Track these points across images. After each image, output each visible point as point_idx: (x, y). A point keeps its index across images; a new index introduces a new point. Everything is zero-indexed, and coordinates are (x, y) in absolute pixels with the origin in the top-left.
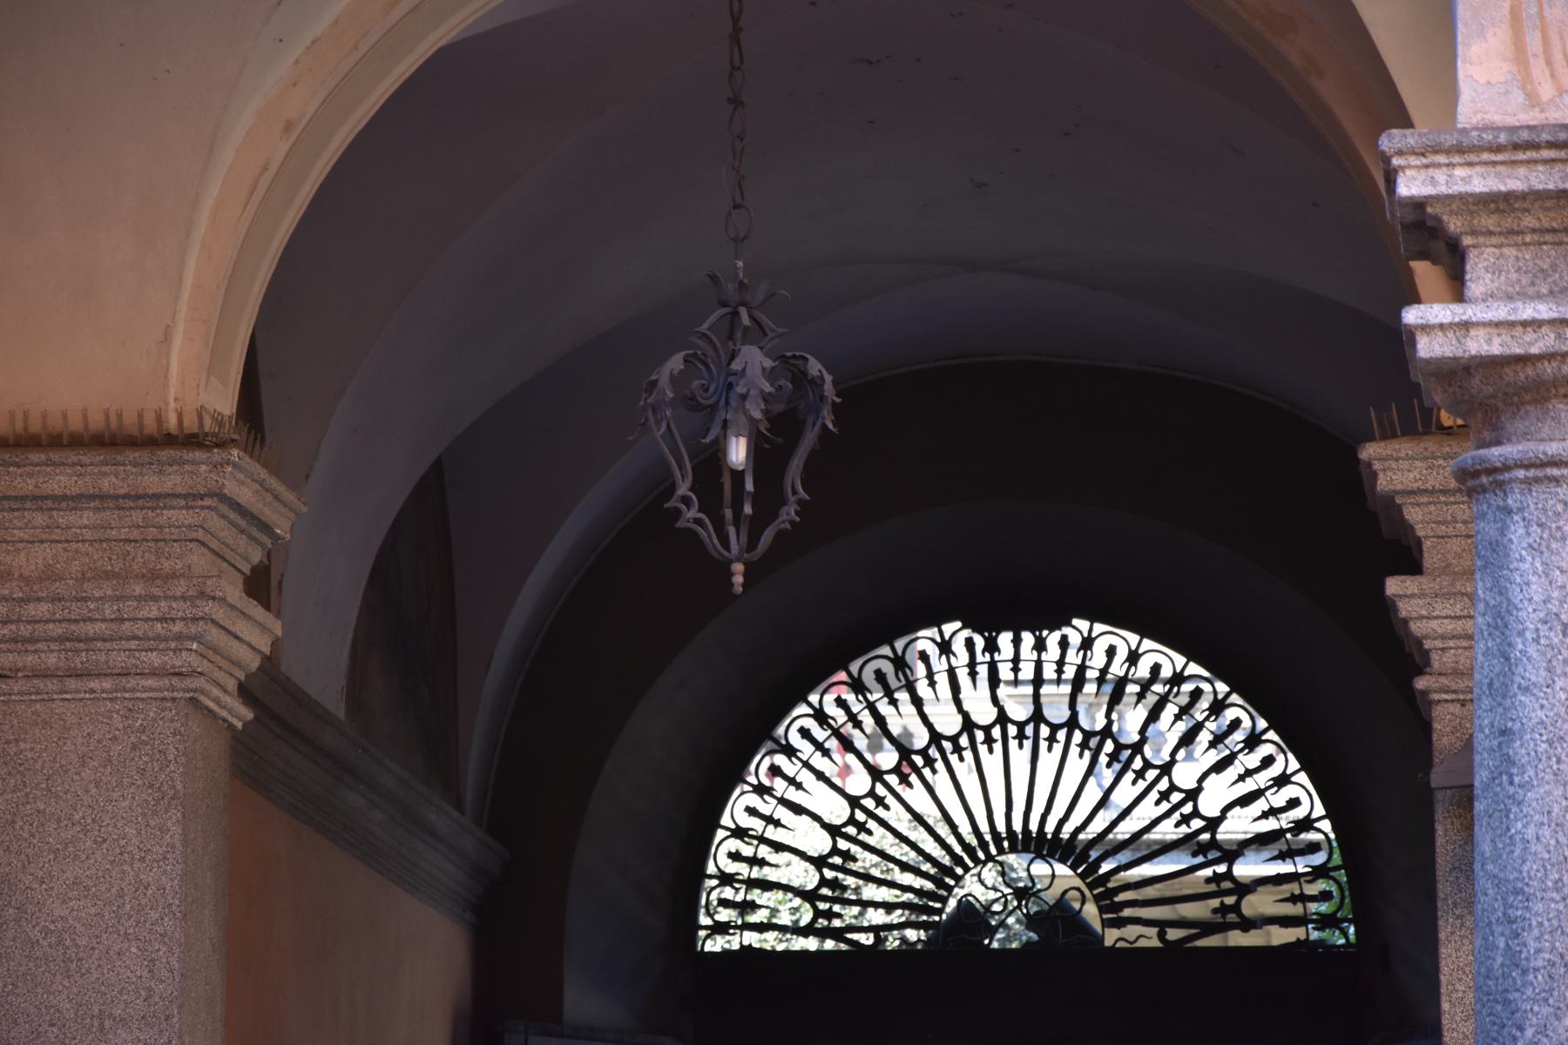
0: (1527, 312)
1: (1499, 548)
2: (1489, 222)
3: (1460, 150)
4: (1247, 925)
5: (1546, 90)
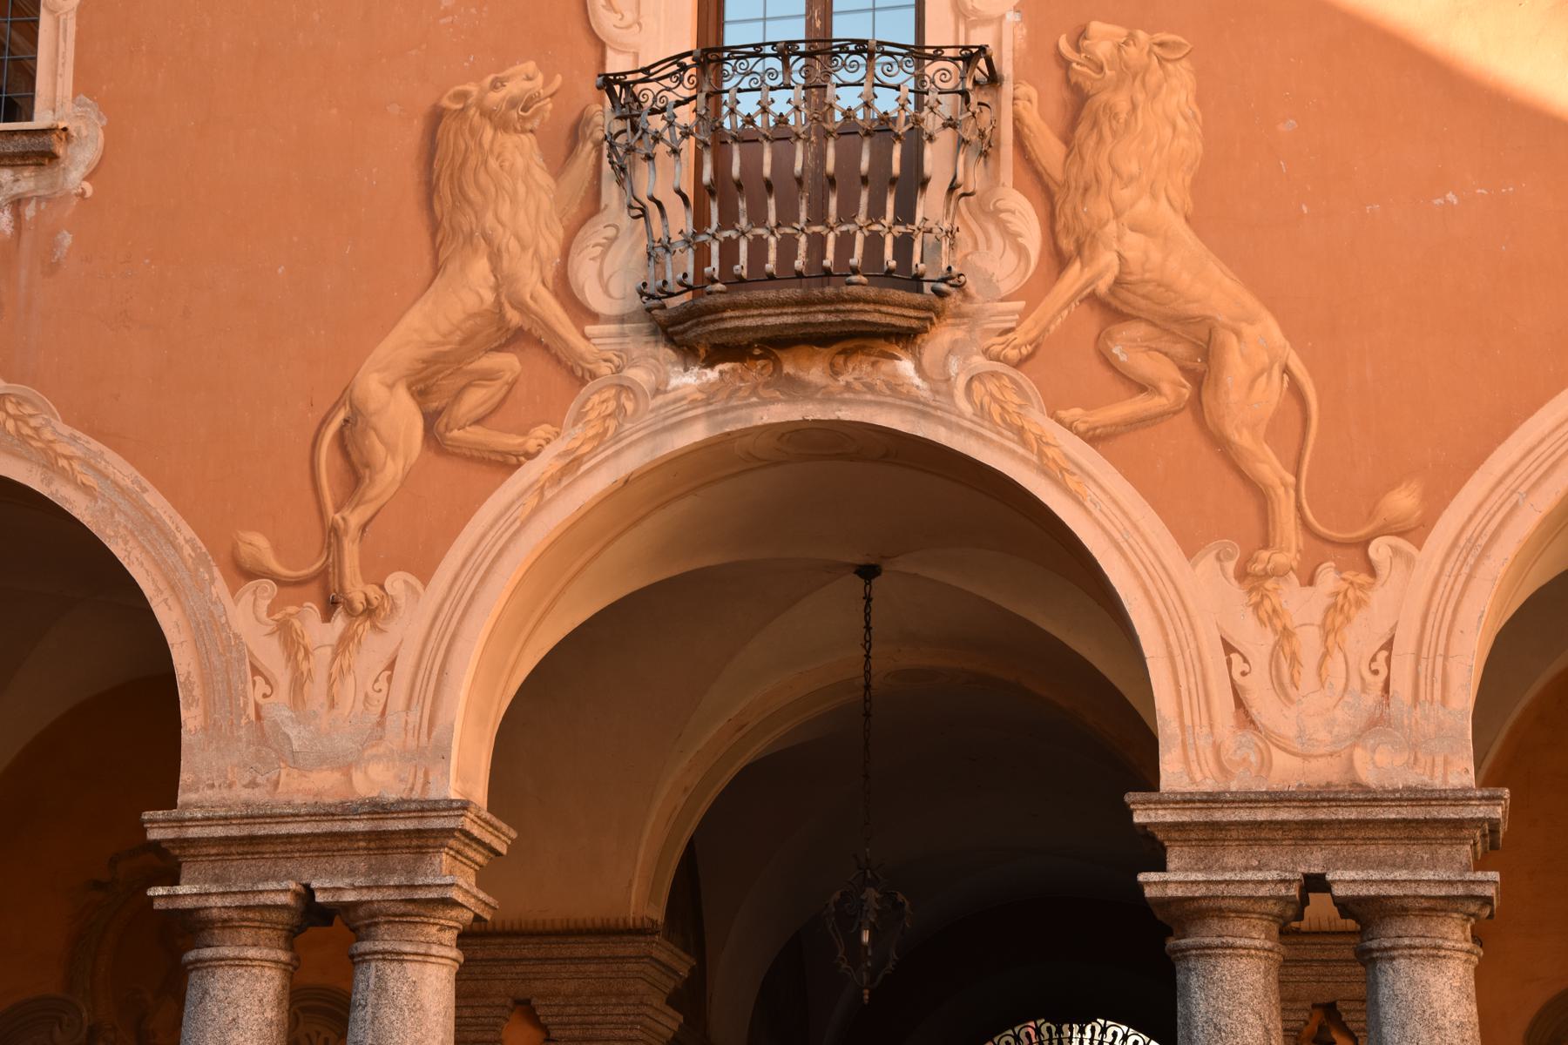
0: (1193, 877)
2: (1175, 835)
5: (1198, 777)
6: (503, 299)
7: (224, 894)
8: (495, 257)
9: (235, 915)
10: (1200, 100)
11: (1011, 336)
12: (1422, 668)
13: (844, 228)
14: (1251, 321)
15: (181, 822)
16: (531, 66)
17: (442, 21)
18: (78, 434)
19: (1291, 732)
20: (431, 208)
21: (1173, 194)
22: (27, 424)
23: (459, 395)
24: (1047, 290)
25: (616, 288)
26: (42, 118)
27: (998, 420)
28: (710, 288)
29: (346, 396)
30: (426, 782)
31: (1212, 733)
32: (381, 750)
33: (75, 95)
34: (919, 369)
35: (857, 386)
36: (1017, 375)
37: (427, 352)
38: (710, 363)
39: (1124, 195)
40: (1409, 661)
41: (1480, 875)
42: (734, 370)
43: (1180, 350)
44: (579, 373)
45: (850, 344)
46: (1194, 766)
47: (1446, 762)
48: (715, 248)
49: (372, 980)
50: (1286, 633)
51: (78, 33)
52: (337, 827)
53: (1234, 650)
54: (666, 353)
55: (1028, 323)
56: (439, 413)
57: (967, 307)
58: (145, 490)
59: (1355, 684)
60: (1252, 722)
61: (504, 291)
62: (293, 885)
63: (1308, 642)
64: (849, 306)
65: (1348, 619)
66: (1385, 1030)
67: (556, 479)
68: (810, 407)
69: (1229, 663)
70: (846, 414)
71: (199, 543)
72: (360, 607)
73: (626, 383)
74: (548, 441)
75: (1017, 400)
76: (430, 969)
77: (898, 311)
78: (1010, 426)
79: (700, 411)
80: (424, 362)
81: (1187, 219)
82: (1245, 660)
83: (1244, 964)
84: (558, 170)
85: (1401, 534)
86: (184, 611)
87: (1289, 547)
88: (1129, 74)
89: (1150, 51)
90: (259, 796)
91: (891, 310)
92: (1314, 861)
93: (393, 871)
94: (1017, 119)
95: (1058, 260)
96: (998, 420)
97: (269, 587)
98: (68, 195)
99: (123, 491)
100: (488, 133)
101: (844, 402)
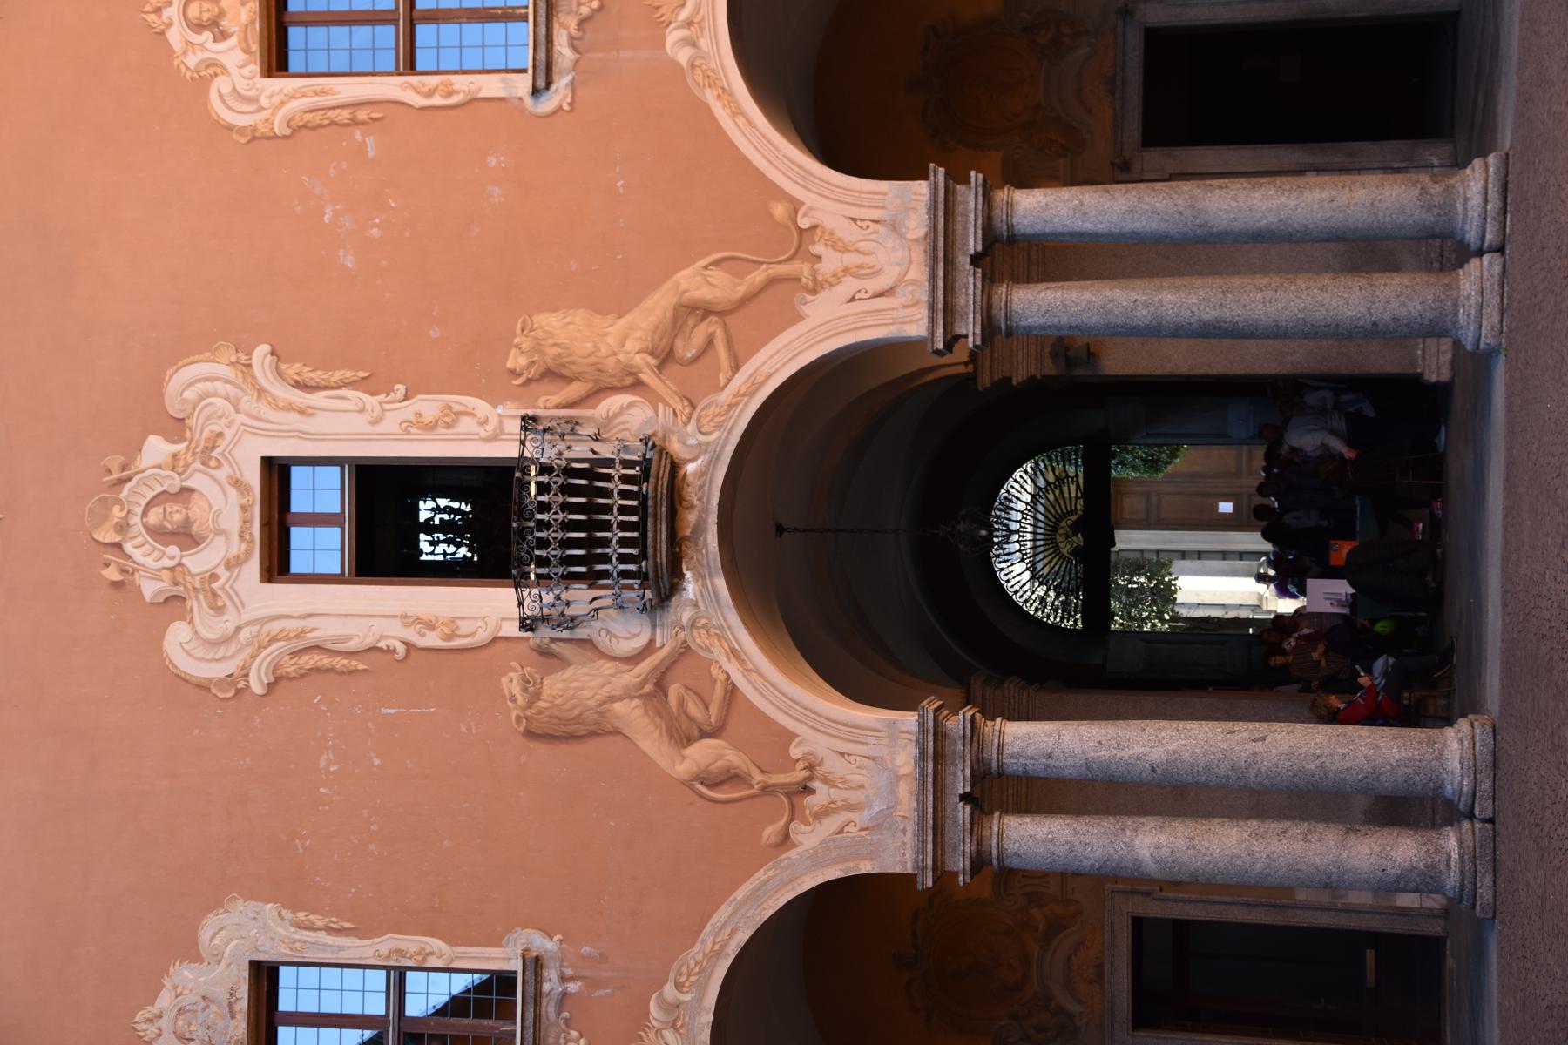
0: (971, 320)
1: (1025, 328)
2: (949, 329)
3: (933, 334)
4: (1077, 475)
5: (919, 316)
6: (637, 694)
7: (964, 843)
8: (613, 699)
9: (975, 837)
10: (555, 310)
11: (678, 411)
12: (867, 204)
13: (616, 495)
14: (678, 285)
15: (924, 868)
16: (504, 680)
17: (474, 731)
18: (700, 939)
19: (897, 270)
20: (582, 737)
21: (605, 325)
22: (692, 969)
23: (691, 719)
24: (654, 391)
25: (636, 630)
26: (516, 965)
27: (723, 418)
28: (644, 570)
29: (687, 784)
30: (908, 732)
31: (897, 309)
32: (888, 758)
33: (501, 946)
34: (693, 460)
35: (700, 494)
36: (698, 410)
37: (665, 738)
38: (682, 576)
39: (604, 350)
40: (863, 210)
41: (973, 180)
42: (686, 563)
43: (691, 322)
44: (683, 650)
45: (676, 497)
46: (914, 318)
47: (915, 194)
48: (622, 567)
49: (1013, 761)
50: (846, 270)
51: (465, 945)
52: (930, 780)
53: (854, 297)
54: (675, 601)
55: (671, 402)
56: (701, 730)
57: (660, 434)
58: (735, 899)
59: (874, 237)
60: (892, 288)
61: (632, 694)
62: (961, 804)
63: (851, 259)
64: (659, 494)
65: (840, 239)
66: (1047, 231)
67: (742, 662)
68: (710, 520)
69: (860, 299)
70: (715, 500)
71: (767, 866)
72: (808, 773)
73: (690, 623)
74: (720, 667)
75: (713, 408)
76: (1008, 730)
77: (662, 469)
78: (727, 411)
79: (708, 582)
80: (670, 739)
81: (620, 317)
82: (859, 291)
83: (1015, 298)
84: (566, 664)
85: (796, 212)
86: (806, 874)
87: (802, 269)
88: (538, 347)
89: (526, 336)
90: (911, 827)
91: (661, 472)
92: (963, 261)
93: (954, 751)
94: (557, 407)
95: (637, 385)
96: (723, 418)
97: (794, 825)
98: (561, 950)
99: (735, 911)
100: (541, 704)
101: (708, 502)
